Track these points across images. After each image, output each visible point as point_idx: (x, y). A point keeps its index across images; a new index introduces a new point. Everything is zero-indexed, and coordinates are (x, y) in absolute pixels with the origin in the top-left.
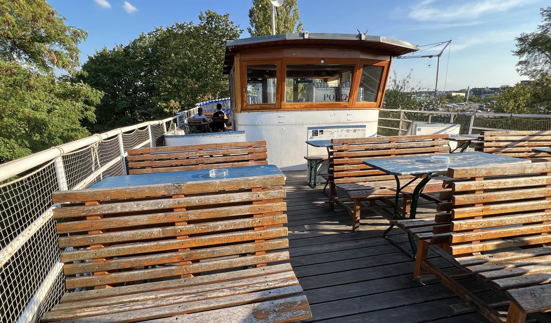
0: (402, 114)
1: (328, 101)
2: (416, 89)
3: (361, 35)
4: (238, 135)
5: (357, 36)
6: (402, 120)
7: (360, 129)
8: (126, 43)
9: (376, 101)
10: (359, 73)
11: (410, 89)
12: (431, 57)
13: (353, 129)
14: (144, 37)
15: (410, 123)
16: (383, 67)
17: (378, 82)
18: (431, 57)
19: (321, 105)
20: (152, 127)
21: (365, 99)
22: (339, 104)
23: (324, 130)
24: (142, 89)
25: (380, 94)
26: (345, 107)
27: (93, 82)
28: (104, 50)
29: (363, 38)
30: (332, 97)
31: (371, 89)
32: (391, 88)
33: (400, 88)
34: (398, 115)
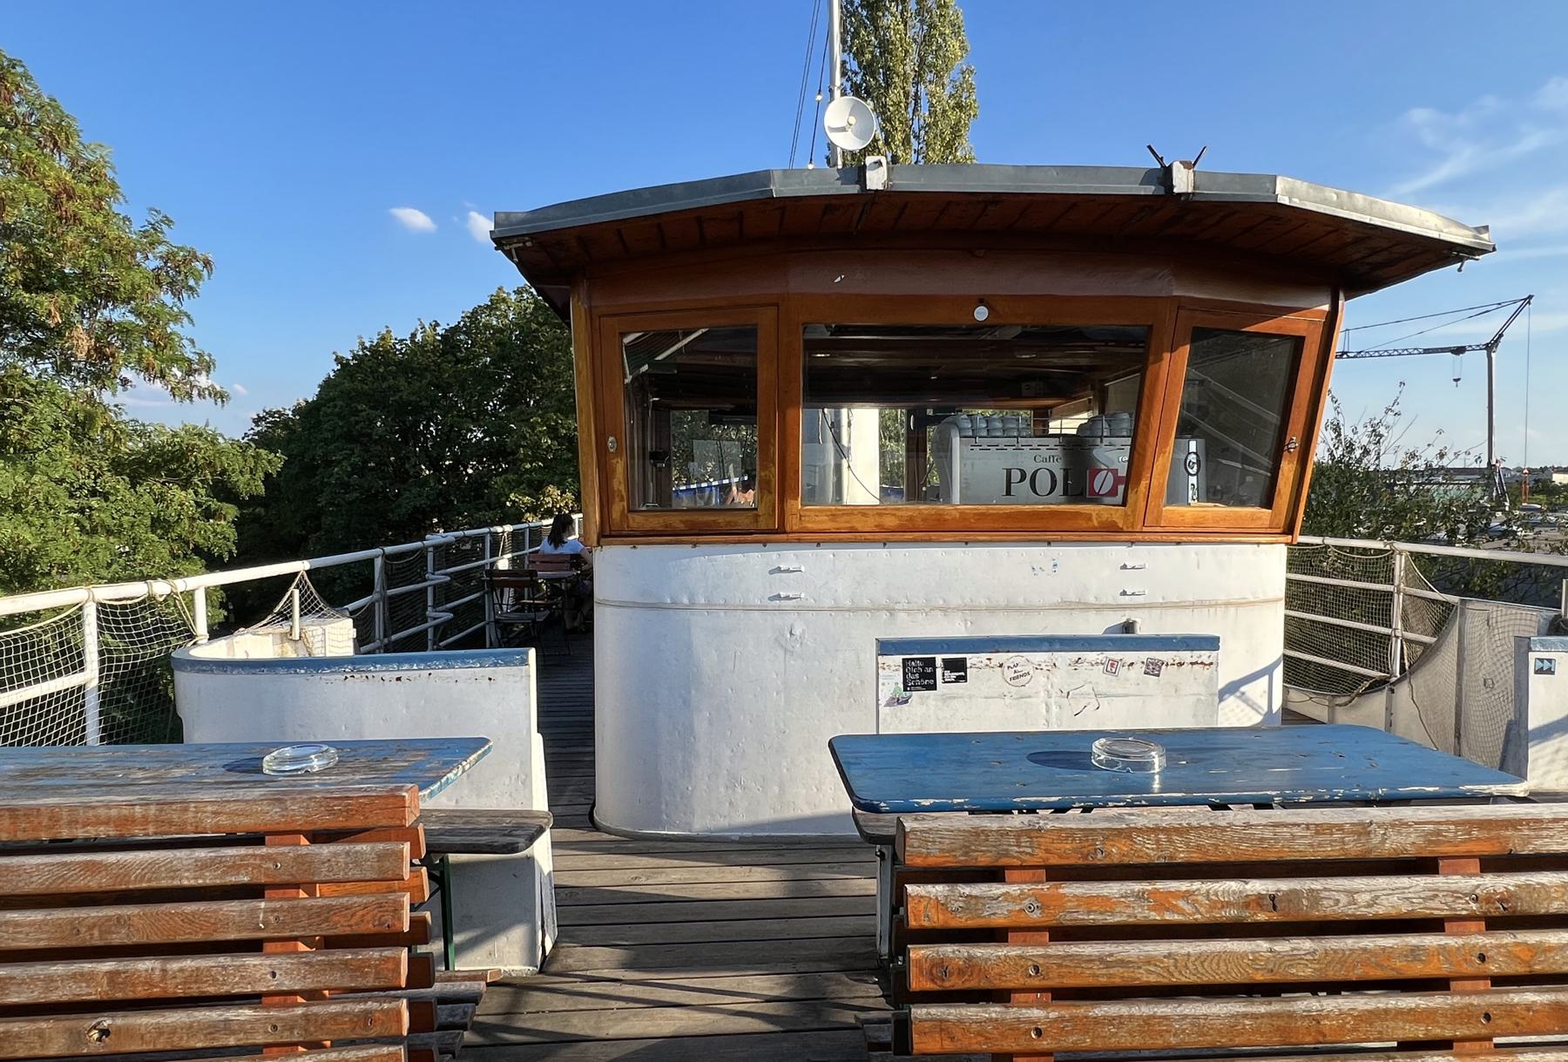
0: (1400, 563)
1: (1024, 502)
2: (1428, 456)
3: (1168, 171)
4: (489, 671)
5: (1149, 176)
6: (1402, 585)
7: (1186, 656)
8: (450, 318)
9: (1268, 503)
10: (1174, 370)
11: (1402, 456)
12: (1459, 351)
13: (1145, 655)
14: (504, 300)
15: (1448, 607)
16: (1298, 342)
17: (1274, 418)
18: (1459, 351)
19: (982, 516)
20: (104, 610)
21: (1214, 492)
22: (1077, 514)
23: (971, 659)
24: (478, 451)
25: (1288, 469)
26: (1109, 533)
27: (338, 431)
28: (383, 338)
29: (1182, 181)
30: (1044, 481)
31: (1240, 447)
32: (1326, 459)
33: (1358, 453)
34: (1379, 566)
